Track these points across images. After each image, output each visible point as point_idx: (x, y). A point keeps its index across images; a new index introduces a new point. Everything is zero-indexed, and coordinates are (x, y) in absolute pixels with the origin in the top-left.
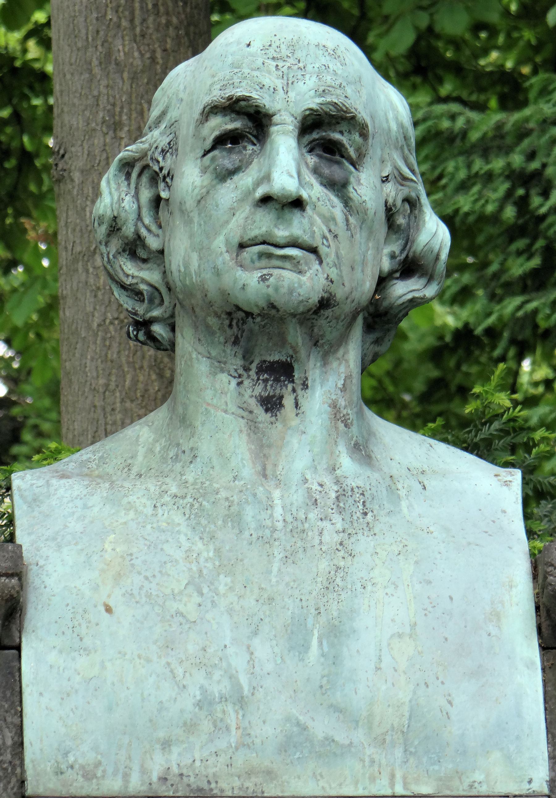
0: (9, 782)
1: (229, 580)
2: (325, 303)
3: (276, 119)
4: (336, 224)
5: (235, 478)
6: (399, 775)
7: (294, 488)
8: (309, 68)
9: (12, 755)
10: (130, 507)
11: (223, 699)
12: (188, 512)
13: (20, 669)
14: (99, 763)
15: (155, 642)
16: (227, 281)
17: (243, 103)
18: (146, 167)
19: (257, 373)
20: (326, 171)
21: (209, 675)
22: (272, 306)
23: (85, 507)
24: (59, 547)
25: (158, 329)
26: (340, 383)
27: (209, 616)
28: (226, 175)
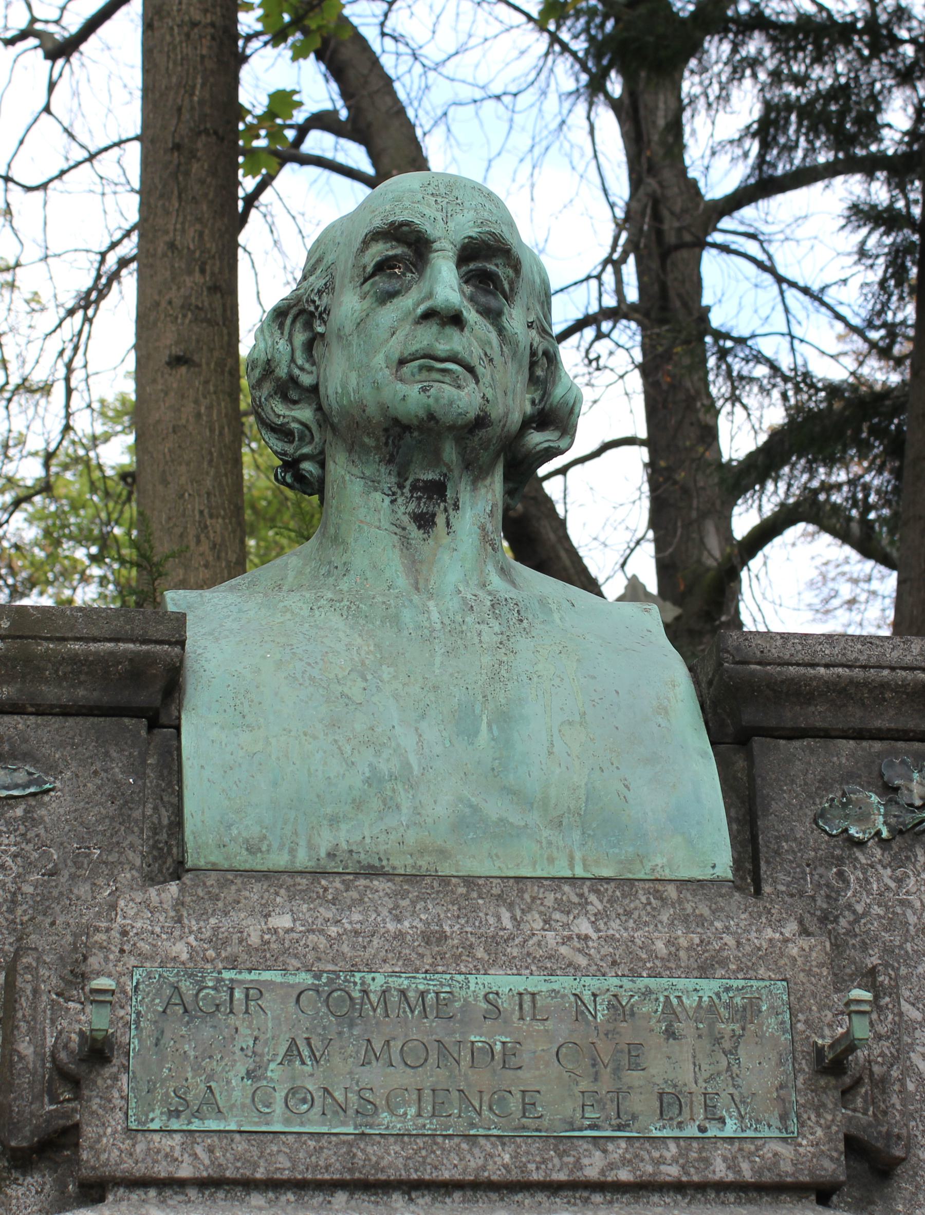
0: (165, 863)
1: (392, 670)
2: (481, 421)
3: (436, 246)
4: (492, 348)
5: (389, 587)
6: (578, 856)
7: (449, 597)
8: (467, 204)
9: (168, 835)
10: (286, 610)
11: (392, 777)
12: (345, 613)
13: (179, 749)
14: (265, 837)
15: (321, 721)
16: (387, 395)
17: (405, 229)
18: (302, 312)
19: (411, 491)
20: (482, 299)
21: (378, 753)
22: (431, 416)
23: (240, 611)
24: (217, 639)
25: (307, 466)
26: (488, 509)
27: (375, 699)
28: (387, 297)
